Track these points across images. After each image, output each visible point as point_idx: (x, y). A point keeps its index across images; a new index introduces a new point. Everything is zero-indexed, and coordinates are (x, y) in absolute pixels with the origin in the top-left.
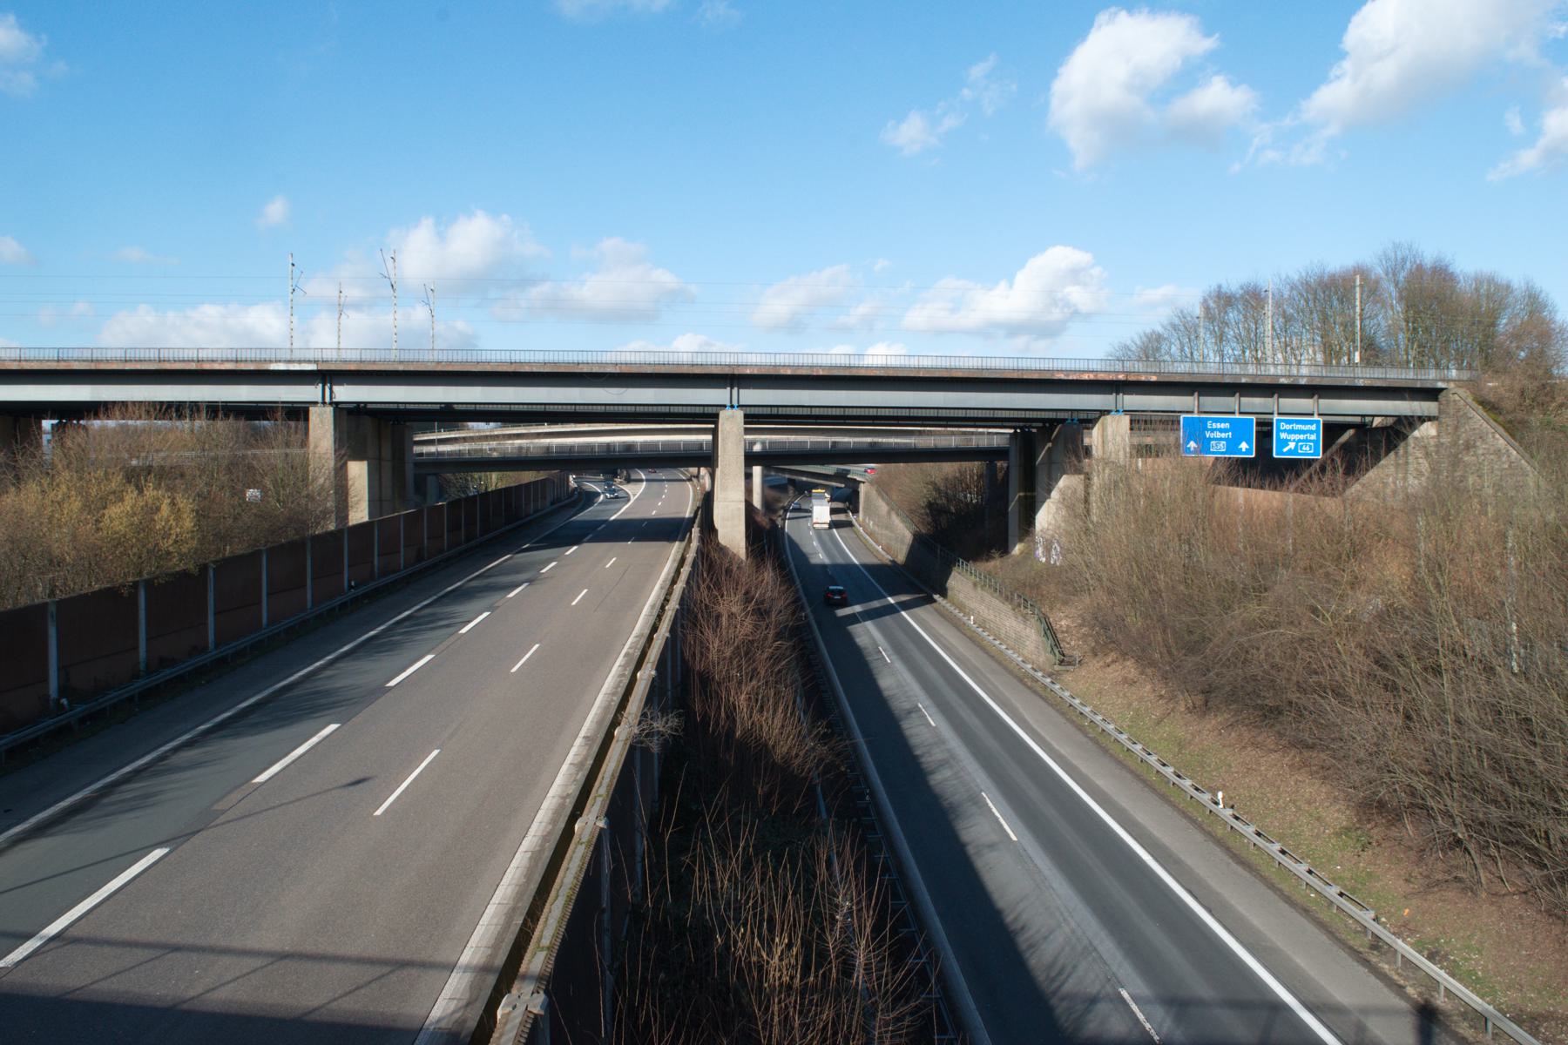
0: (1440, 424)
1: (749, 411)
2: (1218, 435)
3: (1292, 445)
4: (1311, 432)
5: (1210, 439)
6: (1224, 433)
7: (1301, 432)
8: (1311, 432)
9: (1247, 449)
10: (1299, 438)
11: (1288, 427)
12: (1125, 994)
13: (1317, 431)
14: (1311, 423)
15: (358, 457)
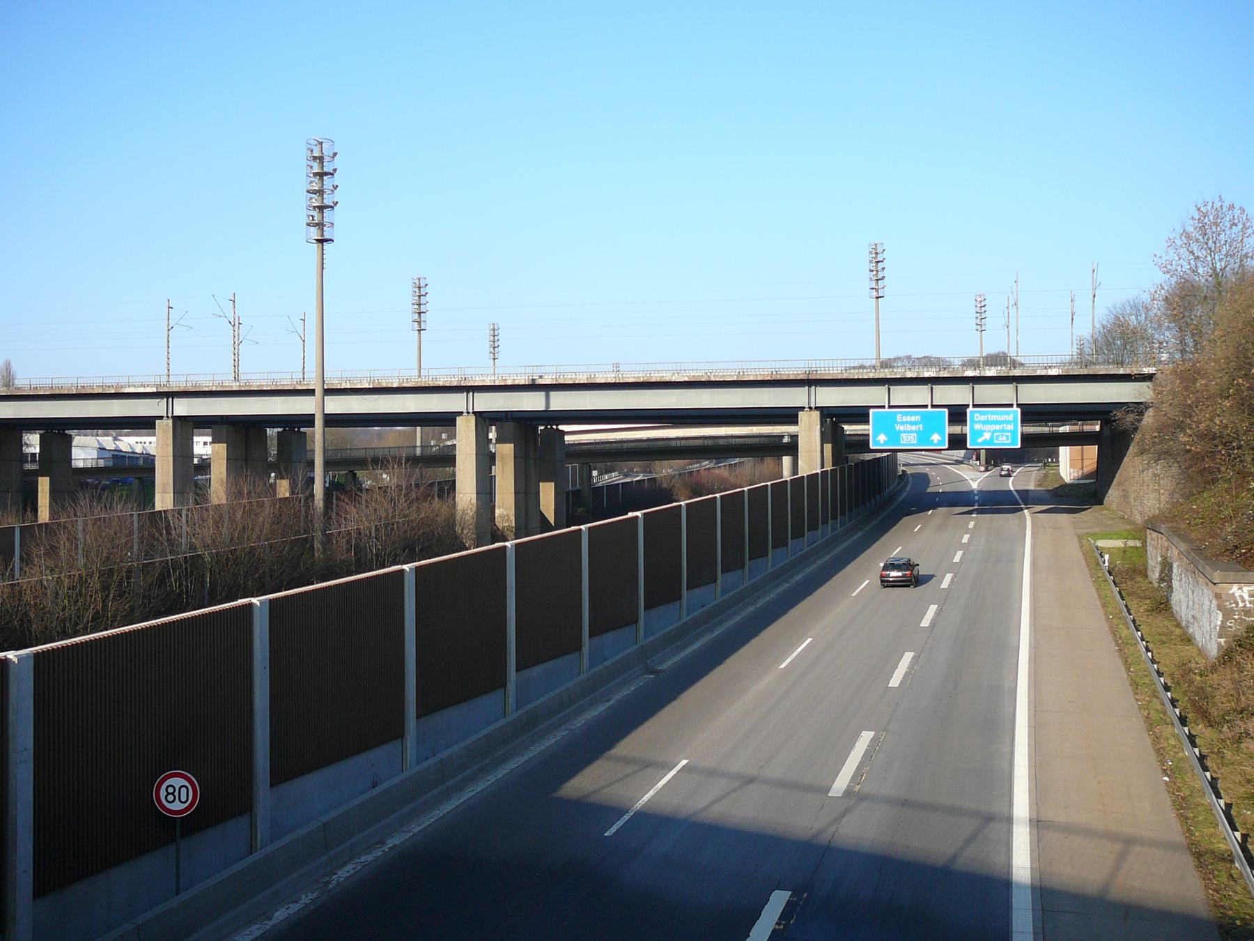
2: (909, 428)
3: (987, 436)
4: (1008, 422)
5: (900, 432)
7: (996, 422)
8: (1008, 422)
11: (983, 418)
13: (1015, 418)
14: (1008, 413)
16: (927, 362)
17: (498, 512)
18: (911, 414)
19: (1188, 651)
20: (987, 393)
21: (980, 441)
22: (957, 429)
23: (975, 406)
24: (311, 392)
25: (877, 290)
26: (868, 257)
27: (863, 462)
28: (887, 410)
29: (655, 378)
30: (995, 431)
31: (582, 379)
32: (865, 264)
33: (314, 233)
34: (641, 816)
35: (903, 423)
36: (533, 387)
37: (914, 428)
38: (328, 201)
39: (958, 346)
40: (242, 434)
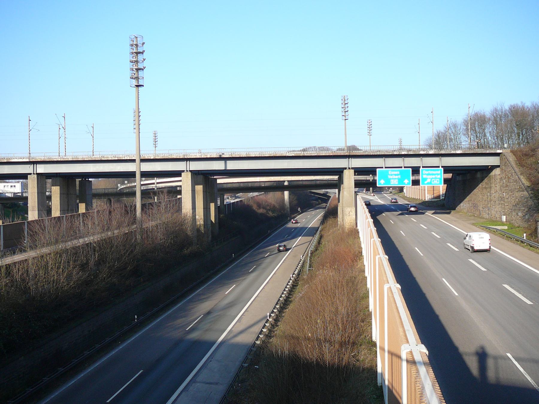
0: (502, 169)
1: (356, 170)
2: (394, 177)
3: (429, 180)
4: (438, 174)
5: (391, 179)
8: (438, 174)
11: (427, 172)
12: (509, 355)
15: (198, 184)
16: (322, 149)
17: (197, 217)
18: (395, 171)
21: (426, 182)
22: (416, 178)
23: (423, 167)
24: (134, 161)
25: (345, 116)
26: (341, 102)
27: (79, 190)
28: (384, 169)
29: (278, 155)
31: (244, 155)
33: (134, 82)
34: (257, 356)
35: (392, 175)
36: (220, 159)
37: (396, 177)
38: (140, 66)
39: (416, 141)
40: (66, 180)
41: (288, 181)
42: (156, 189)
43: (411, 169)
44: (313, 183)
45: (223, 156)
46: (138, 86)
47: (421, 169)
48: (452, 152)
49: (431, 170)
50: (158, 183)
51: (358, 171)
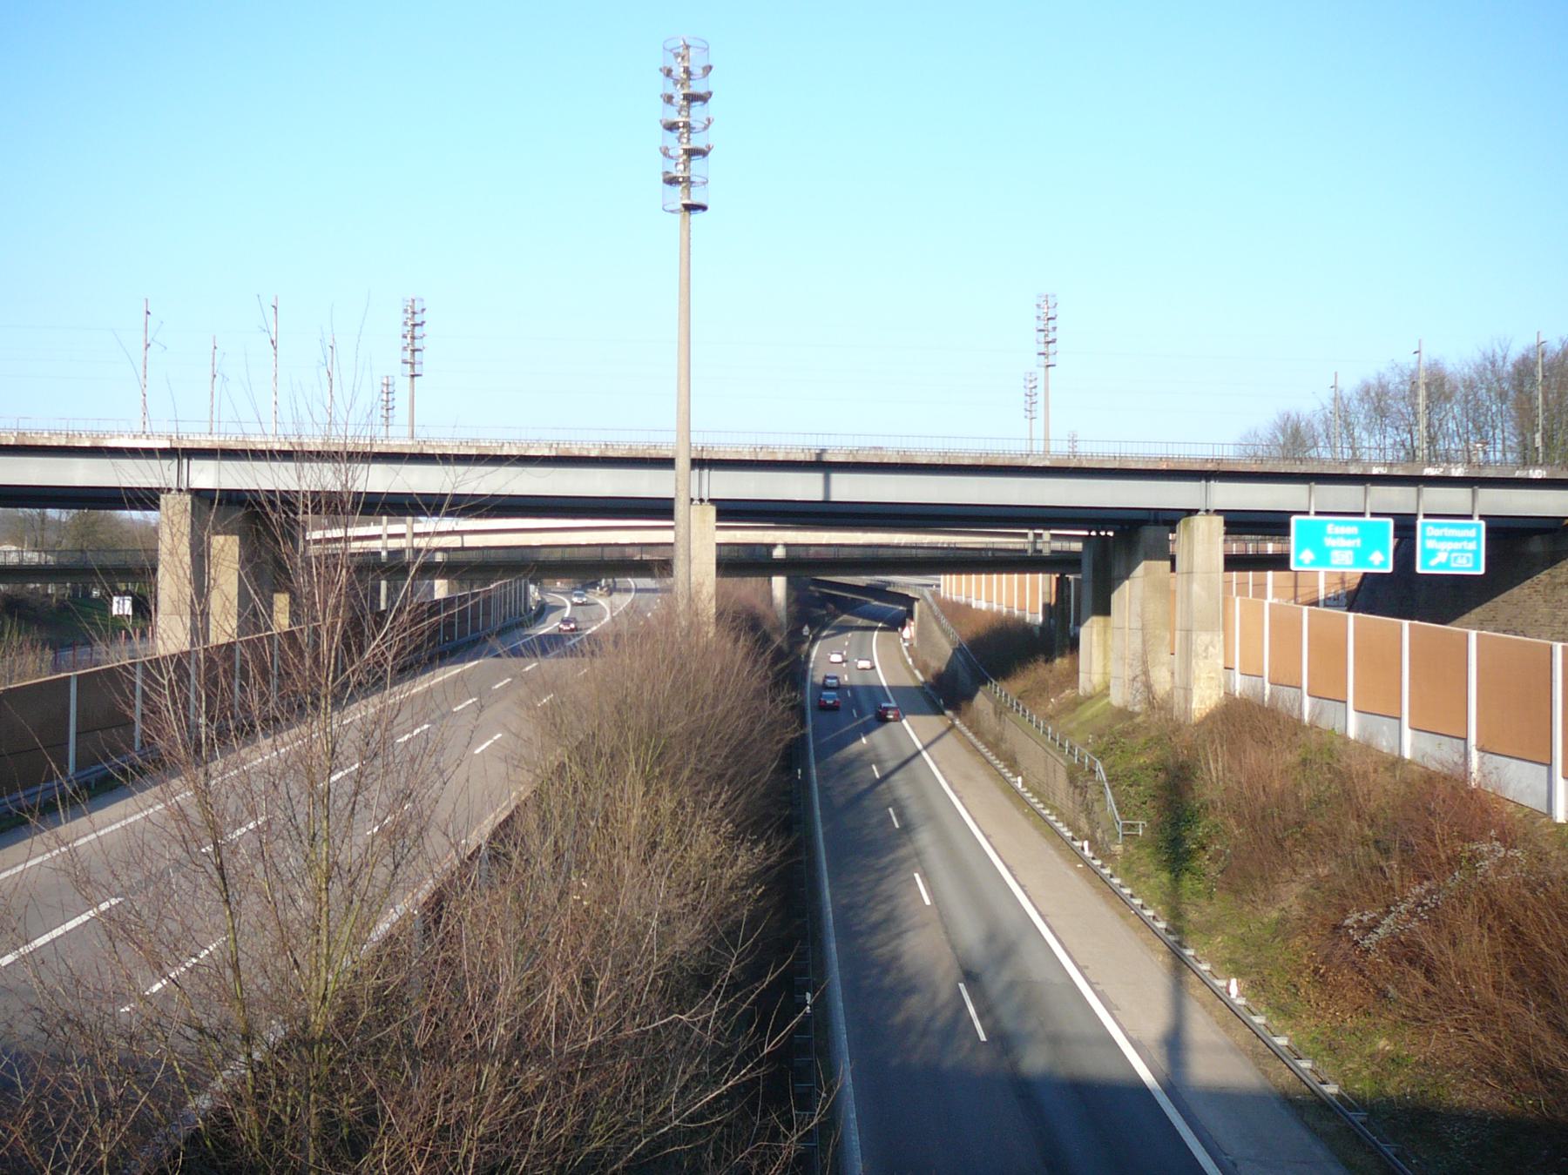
1: (1234, 518)
3: (1442, 557)
4: (1469, 539)
5: (1330, 549)
6: (1339, 545)
8: (1469, 539)
9: (1382, 561)
10: (1451, 549)
11: (1438, 532)
13: (1477, 538)
14: (1470, 527)
19: (529, 804)
20: (1437, 498)
21: (1433, 562)
23: (1426, 516)
26: (401, 317)
28: (1312, 517)
30: (1453, 551)
32: (395, 325)
35: (1335, 536)
37: (1350, 543)
41: (786, 545)
42: (384, 554)
43: (1391, 521)
44: (830, 554)
45: (827, 458)
46: (690, 208)
47: (1420, 521)
48: (1518, 474)
49: (1450, 526)
50: (391, 536)
51: (1238, 523)
